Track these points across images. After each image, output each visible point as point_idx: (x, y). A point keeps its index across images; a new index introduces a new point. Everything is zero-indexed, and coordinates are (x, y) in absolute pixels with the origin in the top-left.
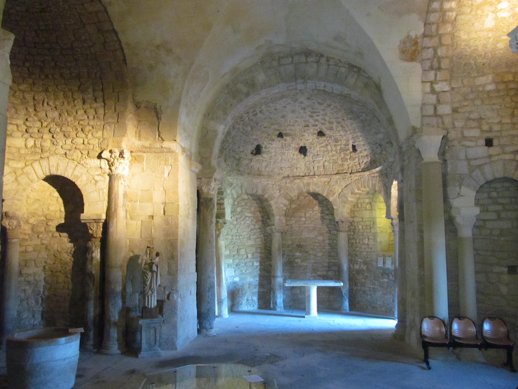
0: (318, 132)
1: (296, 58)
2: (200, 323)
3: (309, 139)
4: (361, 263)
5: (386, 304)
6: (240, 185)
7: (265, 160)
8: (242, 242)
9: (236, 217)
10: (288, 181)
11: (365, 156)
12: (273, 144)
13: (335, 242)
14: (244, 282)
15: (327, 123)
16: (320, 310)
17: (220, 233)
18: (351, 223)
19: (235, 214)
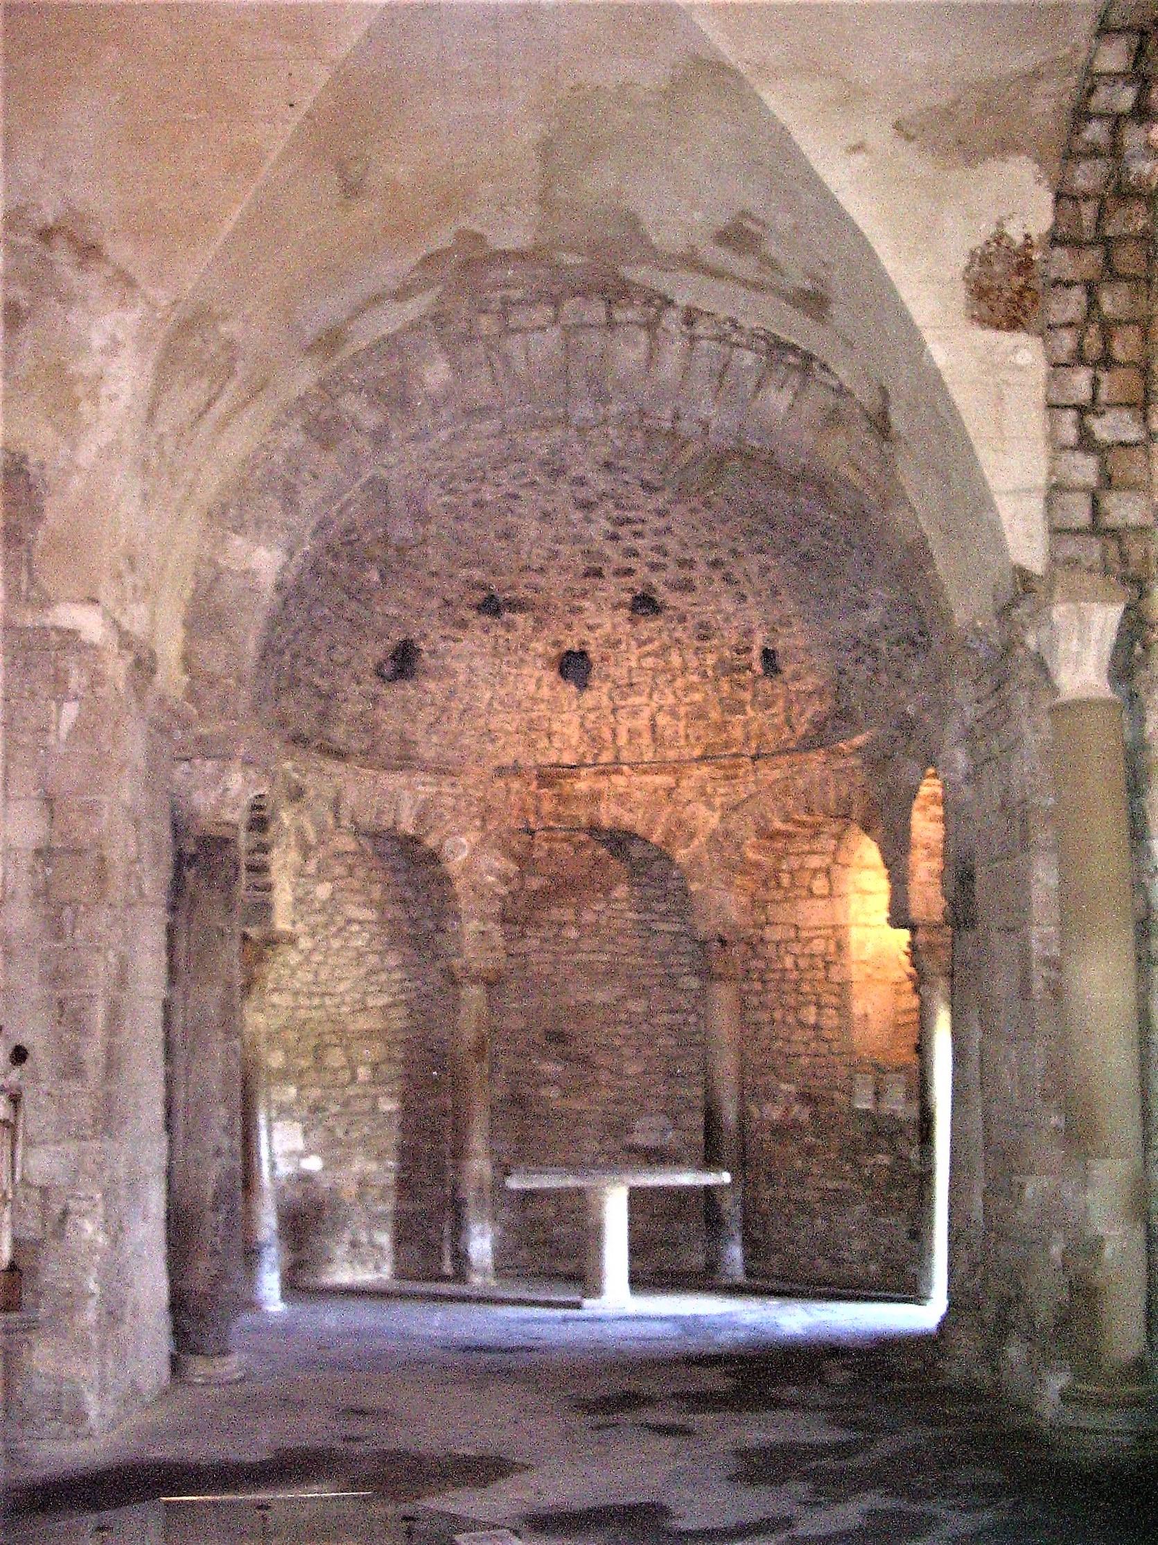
0: (636, 598)
1: (569, 305)
2: (180, 1334)
3: (599, 626)
6: (331, 794)
7: (428, 699)
11: (810, 694)
15: (673, 567)
16: (639, 1282)
19: (304, 908)
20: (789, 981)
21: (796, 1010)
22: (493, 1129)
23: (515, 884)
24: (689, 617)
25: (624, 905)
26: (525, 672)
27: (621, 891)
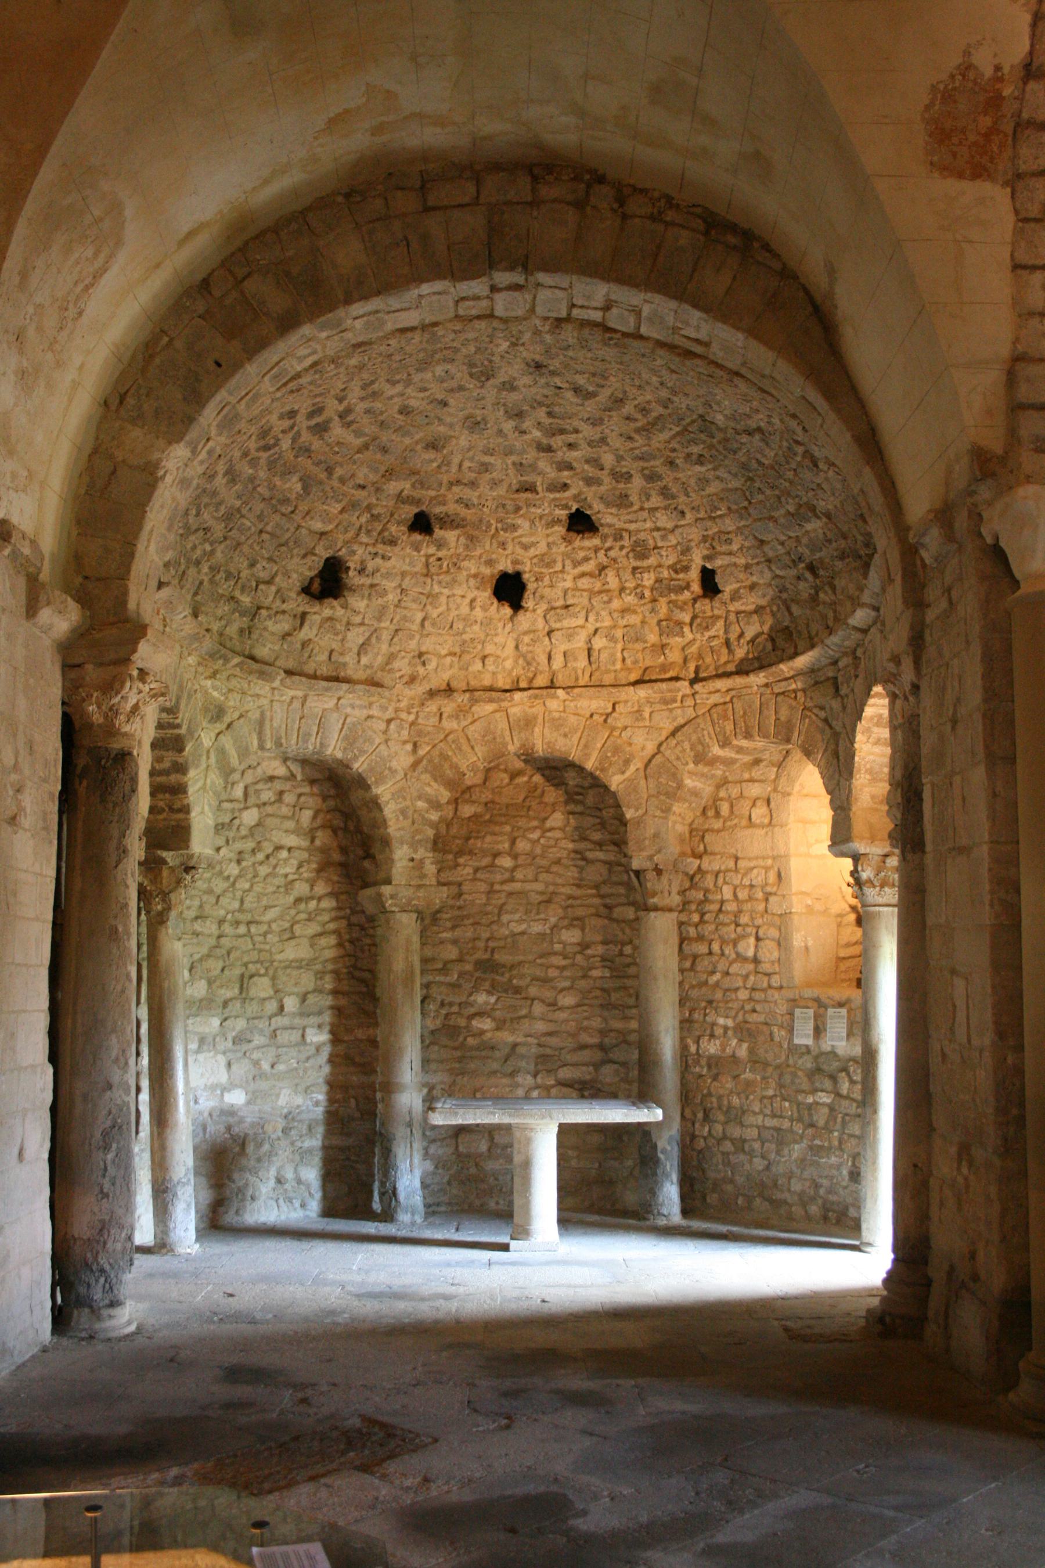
3: (534, 544)
4: (730, 1033)
5: (822, 1191)
6: (255, 715)
7: (357, 619)
8: (260, 951)
9: (239, 846)
10: (449, 707)
12: (390, 558)
13: (628, 950)
14: (267, 1108)
17: (169, 909)
18: (692, 878)
20: (728, 913)
21: (735, 943)
22: (425, 1062)
23: (449, 813)
24: (625, 535)
25: (558, 834)
26: (456, 592)
27: (557, 819)
